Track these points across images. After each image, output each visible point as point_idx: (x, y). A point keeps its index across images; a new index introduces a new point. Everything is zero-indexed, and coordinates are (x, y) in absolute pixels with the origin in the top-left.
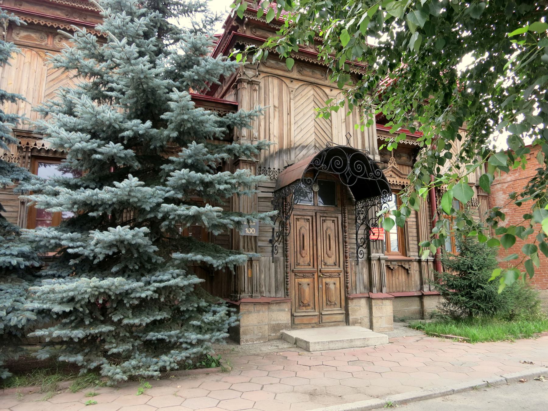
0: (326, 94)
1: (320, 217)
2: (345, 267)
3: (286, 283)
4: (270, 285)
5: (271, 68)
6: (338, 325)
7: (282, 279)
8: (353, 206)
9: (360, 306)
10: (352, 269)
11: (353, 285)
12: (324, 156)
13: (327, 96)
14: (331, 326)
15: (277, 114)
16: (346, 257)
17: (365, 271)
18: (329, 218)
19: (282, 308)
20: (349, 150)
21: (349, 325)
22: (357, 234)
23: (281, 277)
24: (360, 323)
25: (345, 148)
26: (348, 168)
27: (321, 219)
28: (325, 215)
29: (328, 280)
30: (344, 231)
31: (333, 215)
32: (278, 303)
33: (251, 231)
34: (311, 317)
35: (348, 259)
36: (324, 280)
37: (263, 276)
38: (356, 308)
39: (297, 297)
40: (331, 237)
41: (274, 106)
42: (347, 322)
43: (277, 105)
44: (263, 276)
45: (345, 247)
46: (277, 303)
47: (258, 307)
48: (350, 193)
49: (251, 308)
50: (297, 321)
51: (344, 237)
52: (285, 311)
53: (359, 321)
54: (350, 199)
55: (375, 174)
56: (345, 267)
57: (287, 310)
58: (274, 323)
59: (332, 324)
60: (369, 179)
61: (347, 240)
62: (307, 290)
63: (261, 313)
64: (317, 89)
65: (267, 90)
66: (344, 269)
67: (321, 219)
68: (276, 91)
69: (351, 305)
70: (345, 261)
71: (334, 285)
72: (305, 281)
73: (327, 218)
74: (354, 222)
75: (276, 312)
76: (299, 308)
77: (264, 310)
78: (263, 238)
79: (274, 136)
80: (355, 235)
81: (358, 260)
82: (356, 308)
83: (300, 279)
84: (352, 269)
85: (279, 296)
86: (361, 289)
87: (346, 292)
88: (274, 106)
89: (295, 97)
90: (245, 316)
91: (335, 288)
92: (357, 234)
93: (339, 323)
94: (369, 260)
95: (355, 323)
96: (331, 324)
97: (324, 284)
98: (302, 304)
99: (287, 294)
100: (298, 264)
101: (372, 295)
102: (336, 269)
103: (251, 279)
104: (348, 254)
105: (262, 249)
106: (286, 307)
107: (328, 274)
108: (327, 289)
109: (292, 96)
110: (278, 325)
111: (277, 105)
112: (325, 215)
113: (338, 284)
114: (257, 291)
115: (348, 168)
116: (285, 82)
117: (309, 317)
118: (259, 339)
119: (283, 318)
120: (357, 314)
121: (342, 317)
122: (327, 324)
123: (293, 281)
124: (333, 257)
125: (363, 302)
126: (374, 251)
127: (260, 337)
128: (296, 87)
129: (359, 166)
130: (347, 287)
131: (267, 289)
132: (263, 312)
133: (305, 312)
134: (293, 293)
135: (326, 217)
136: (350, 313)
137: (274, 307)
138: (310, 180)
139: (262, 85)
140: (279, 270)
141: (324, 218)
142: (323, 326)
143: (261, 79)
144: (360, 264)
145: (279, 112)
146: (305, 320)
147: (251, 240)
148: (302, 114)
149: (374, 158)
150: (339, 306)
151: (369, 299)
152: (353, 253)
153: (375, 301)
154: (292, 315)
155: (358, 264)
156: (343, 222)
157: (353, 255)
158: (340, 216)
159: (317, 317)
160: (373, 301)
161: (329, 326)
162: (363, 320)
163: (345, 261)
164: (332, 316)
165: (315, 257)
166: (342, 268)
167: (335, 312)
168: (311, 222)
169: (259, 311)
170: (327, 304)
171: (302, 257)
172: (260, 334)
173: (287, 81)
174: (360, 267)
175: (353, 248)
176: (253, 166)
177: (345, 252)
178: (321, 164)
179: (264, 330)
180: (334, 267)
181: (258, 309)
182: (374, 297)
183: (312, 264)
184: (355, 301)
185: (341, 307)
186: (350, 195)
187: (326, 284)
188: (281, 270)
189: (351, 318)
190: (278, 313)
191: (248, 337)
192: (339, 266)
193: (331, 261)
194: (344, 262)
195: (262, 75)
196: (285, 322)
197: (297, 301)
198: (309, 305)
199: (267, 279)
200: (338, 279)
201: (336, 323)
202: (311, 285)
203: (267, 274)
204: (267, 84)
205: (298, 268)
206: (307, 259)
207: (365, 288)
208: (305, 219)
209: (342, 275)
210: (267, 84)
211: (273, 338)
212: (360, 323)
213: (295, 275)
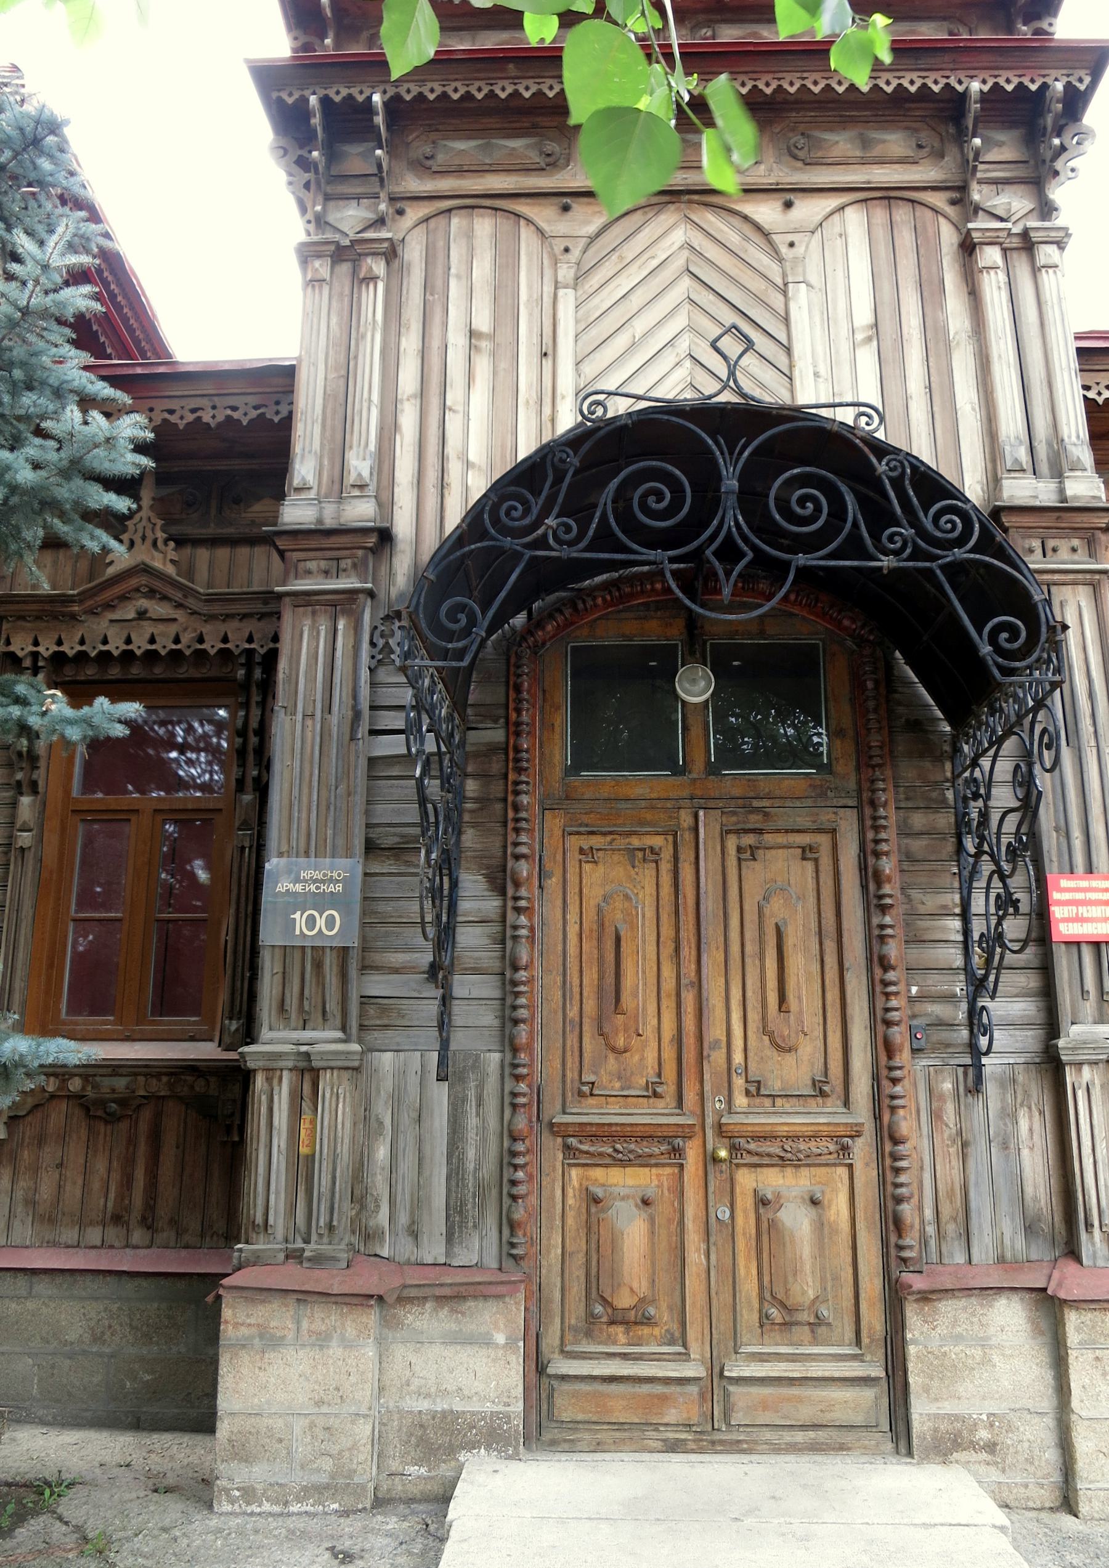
0: (758, 227)
1: (725, 833)
2: (883, 1104)
3: (509, 1191)
4: (419, 1203)
5: (460, 171)
6: (842, 1448)
7: (489, 1168)
8: (939, 759)
9: (983, 1343)
10: (936, 1116)
11: (946, 1211)
12: (558, 480)
13: (765, 234)
14: (793, 1448)
15: (483, 366)
16: (890, 1050)
17: (1031, 1130)
18: (781, 839)
19: (470, 1326)
20: (742, 421)
21: (910, 1453)
22: (965, 916)
23: (480, 1154)
24: (991, 1447)
25: (706, 414)
26: (731, 518)
27: (732, 843)
28: (755, 820)
29: (772, 1180)
30: (874, 903)
31: (803, 821)
32: (455, 1297)
33: (321, 923)
34: (659, 1389)
35: (904, 1057)
36: (746, 1180)
37: (382, 1153)
38: (954, 1351)
39: (577, 1272)
40: (790, 941)
41: (472, 334)
42: (899, 1432)
43: (483, 322)
44: (382, 1153)
45: (879, 989)
46: (441, 1300)
47: (319, 1318)
48: (919, 697)
49: (278, 1317)
50: (566, 1408)
51: (875, 938)
52: (486, 1342)
53: (983, 1434)
54: (919, 726)
55: (921, 532)
56: (883, 1104)
57: (500, 1338)
58: (424, 1405)
59: (799, 1437)
60: (886, 562)
61: (892, 950)
62: (633, 1234)
63: (335, 1350)
64: (711, 220)
65: (440, 271)
66: (877, 1117)
67: (732, 843)
68: (483, 268)
69: (924, 1333)
70: (884, 1075)
71: (816, 1215)
72: (623, 1182)
73: (768, 838)
74: (950, 846)
75: (437, 1350)
76: (589, 1334)
77: (350, 1331)
78: (398, 959)
79: (468, 465)
80: (956, 924)
81: (979, 1067)
82: (954, 1351)
83: (598, 1173)
84: (936, 1116)
85: (466, 1256)
86: (997, 1231)
87: (893, 1257)
88: (472, 334)
89: (578, 281)
90: (245, 1357)
91: (821, 1226)
92: (965, 916)
93: (848, 1438)
94: (1051, 1065)
95: (950, 1444)
96: (788, 1437)
97: (745, 1203)
98: (606, 1313)
99: (510, 1253)
100: (587, 1091)
101: (1070, 1282)
102: (826, 1115)
103: (303, 1169)
104: (898, 1034)
105: (384, 1010)
106: (500, 1322)
107: (774, 1148)
108: (768, 1232)
109: (566, 273)
110: (448, 1418)
111: (483, 322)
112: (755, 820)
113: (838, 1207)
114: (331, 1228)
115: (731, 518)
116: (529, 221)
117: (646, 1389)
118: (317, 1491)
119: (478, 1386)
120: (965, 1388)
121: (864, 1403)
122: (768, 1435)
123: (560, 1185)
124: (809, 1050)
125: (1010, 1318)
126: (1089, 1007)
127: (324, 1479)
128: (592, 229)
129: (802, 501)
130: (892, 1224)
131: (403, 1219)
132: (347, 1345)
133: (625, 1356)
134: (555, 1245)
135: (759, 831)
136: (915, 1380)
137: (425, 1320)
138: (462, 608)
139: (414, 253)
140: (472, 1121)
141: (749, 840)
142: (734, 1447)
143: (410, 232)
144: (991, 1088)
145: (494, 354)
146: (620, 1405)
147: (318, 965)
148: (622, 341)
149: (1061, 491)
150: (850, 1334)
151: (1050, 1307)
152: (941, 1024)
153: (1088, 1317)
154: (537, 1367)
155: (976, 1086)
156: (869, 853)
157: (945, 1035)
158: (848, 826)
159: (693, 1389)
160: (1072, 1319)
161: (777, 1449)
162: (1010, 1429)
163: (884, 1075)
164: (795, 1391)
165: (691, 1051)
166: (862, 1111)
167: (817, 1370)
168: (666, 867)
169: (321, 1340)
170: (764, 1319)
171: (614, 1049)
172: (327, 1464)
173: (544, 214)
174: (994, 1105)
175: (949, 998)
176: (349, 613)
177: (881, 1022)
178: (545, 513)
179: (345, 1442)
180: (813, 1105)
181: (319, 1326)
182: (1076, 1294)
183: (668, 1089)
184: (947, 1308)
185: (858, 1342)
186: (916, 703)
187: (762, 1202)
188: (483, 1126)
189: (922, 1410)
190: (449, 1351)
191: (258, 1473)
192: (846, 1103)
193: (794, 1071)
194: (876, 1078)
195: (414, 213)
196: (489, 1407)
197: (577, 1289)
198: (647, 1321)
199: (407, 1165)
200: (842, 1172)
201: (826, 1438)
202: (664, 1209)
203: (408, 1141)
204: (441, 244)
205: (591, 1113)
206: (647, 1058)
207: (1030, 1229)
208: (631, 852)
209: (862, 1150)
210: (441, 244)
211: (415, 1490)
212: (991, 1447)
213: (567, 1147)
